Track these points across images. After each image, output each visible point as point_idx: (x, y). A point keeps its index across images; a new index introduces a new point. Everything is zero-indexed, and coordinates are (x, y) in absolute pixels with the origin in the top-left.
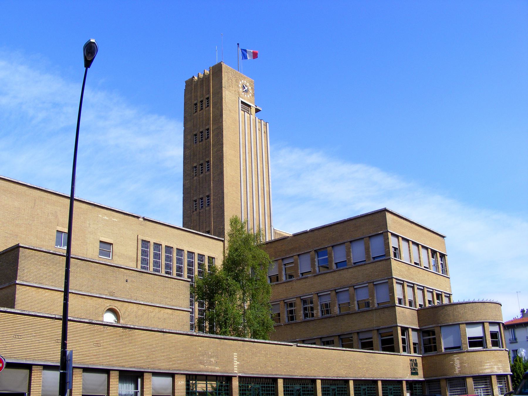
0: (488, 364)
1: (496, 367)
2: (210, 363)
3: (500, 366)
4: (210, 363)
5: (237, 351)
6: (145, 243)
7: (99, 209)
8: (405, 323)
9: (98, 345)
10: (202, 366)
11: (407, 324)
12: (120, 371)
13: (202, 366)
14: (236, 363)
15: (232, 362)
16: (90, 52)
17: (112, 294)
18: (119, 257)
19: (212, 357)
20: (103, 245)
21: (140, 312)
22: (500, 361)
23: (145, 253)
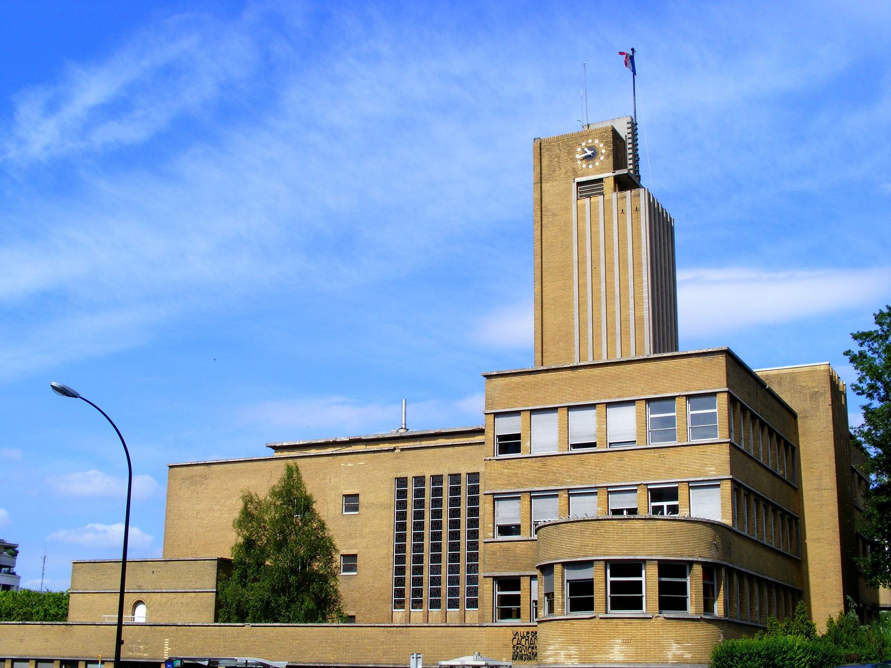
0: (552, 647)
1: (563, 652)
2: (139, 650)
3: (572, 652)
4: (139, 650)
5: (168, 637)
6: (402, 482)
7: (342, 457)
8: (510, 570)
9: (47, 641)
10: (130, 654)
11: (519, 569)
12: (61, 661)
13: (130, 654)
14: (167, 649)
15: (163, 648)
16: (630, 60)
17: (139, 587)
18: (366, 508)
19: (140, 644)
20: (349, 498)
21: (164, 600)
22: (576, 642)
23: (402, 494)
